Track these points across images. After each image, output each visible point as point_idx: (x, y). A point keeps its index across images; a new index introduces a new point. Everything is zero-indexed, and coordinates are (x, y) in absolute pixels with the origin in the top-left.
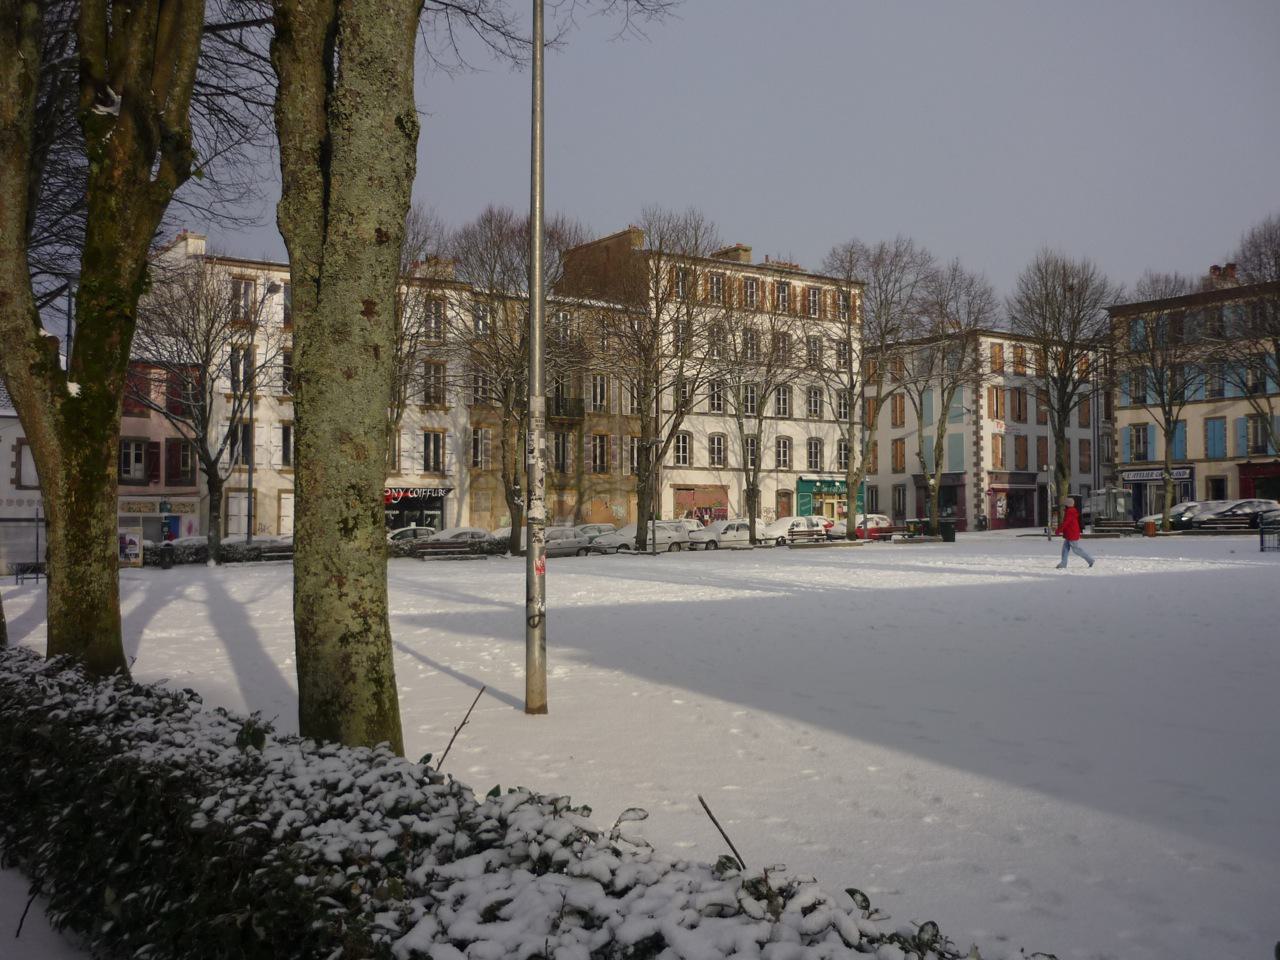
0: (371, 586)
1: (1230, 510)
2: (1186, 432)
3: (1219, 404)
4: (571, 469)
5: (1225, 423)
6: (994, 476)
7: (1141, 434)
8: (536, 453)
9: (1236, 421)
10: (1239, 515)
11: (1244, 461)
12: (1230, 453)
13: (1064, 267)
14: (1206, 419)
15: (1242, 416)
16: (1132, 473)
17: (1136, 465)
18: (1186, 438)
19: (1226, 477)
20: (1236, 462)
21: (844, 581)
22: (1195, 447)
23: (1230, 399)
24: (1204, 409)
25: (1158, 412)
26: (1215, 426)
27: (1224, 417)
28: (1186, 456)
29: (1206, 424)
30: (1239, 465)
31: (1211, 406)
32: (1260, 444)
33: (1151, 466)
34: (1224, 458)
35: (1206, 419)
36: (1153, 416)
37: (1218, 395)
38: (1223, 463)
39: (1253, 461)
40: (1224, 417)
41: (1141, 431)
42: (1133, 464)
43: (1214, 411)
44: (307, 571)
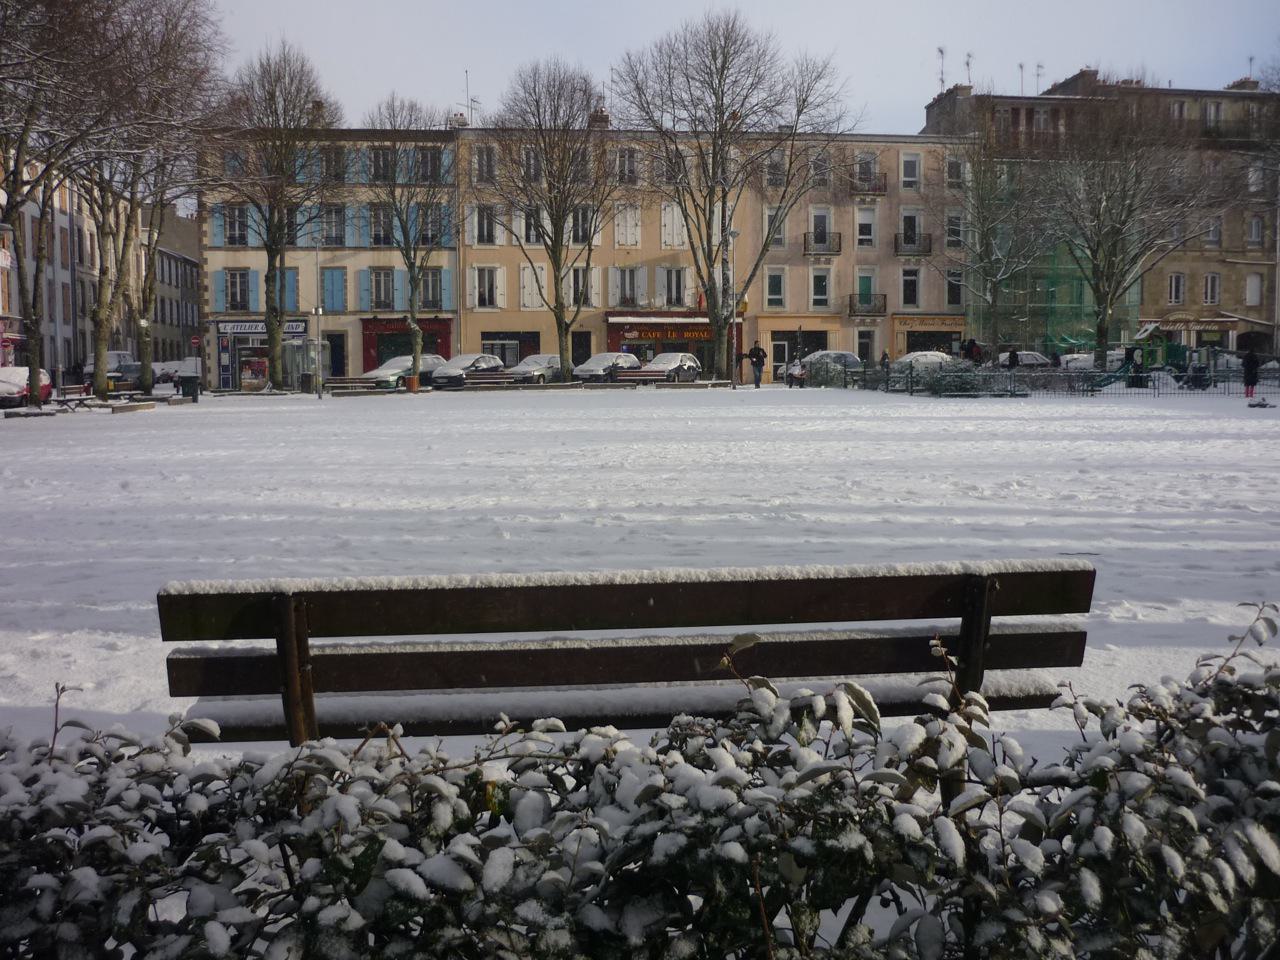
0: (200, 194)
1: (473, 365)
2: (297, 281)
3: (338, 253)
4: (788, 568)
5: (346, 274)
6: (8, 322)
7: (430, 279)
8: (115, 640)
9: (359, 273)
10: (484, 370)
11: (370, 316)
12: (351, 306)
13: (775, 54)
14: (323, 268)
15: (365, 268)
16: (231, 325)
17: (231, 315)
18: (298, 288)
19: (346, 331)
20: (358, 317)
21: (404, 698)
22: (308, 295)
23: (350, 248)
24: (323, 257)
25: (263, 256)
26: (331, 278)
27: (345, 268)
28: (298, 308)
29: (322, 274)
30: (362, 320)
31: (328, 254)
32: (430, 298)
33: (253, 318)
34: (343, 312)
35: (323, 268)
36: (256, 261)
37: (336, 242)
38: (343, 317)
39: (380, 316)
40: (345, 268)
41: (238, 277)
42: (229, 315)
43: (332, 260)
44: (993, 231)
